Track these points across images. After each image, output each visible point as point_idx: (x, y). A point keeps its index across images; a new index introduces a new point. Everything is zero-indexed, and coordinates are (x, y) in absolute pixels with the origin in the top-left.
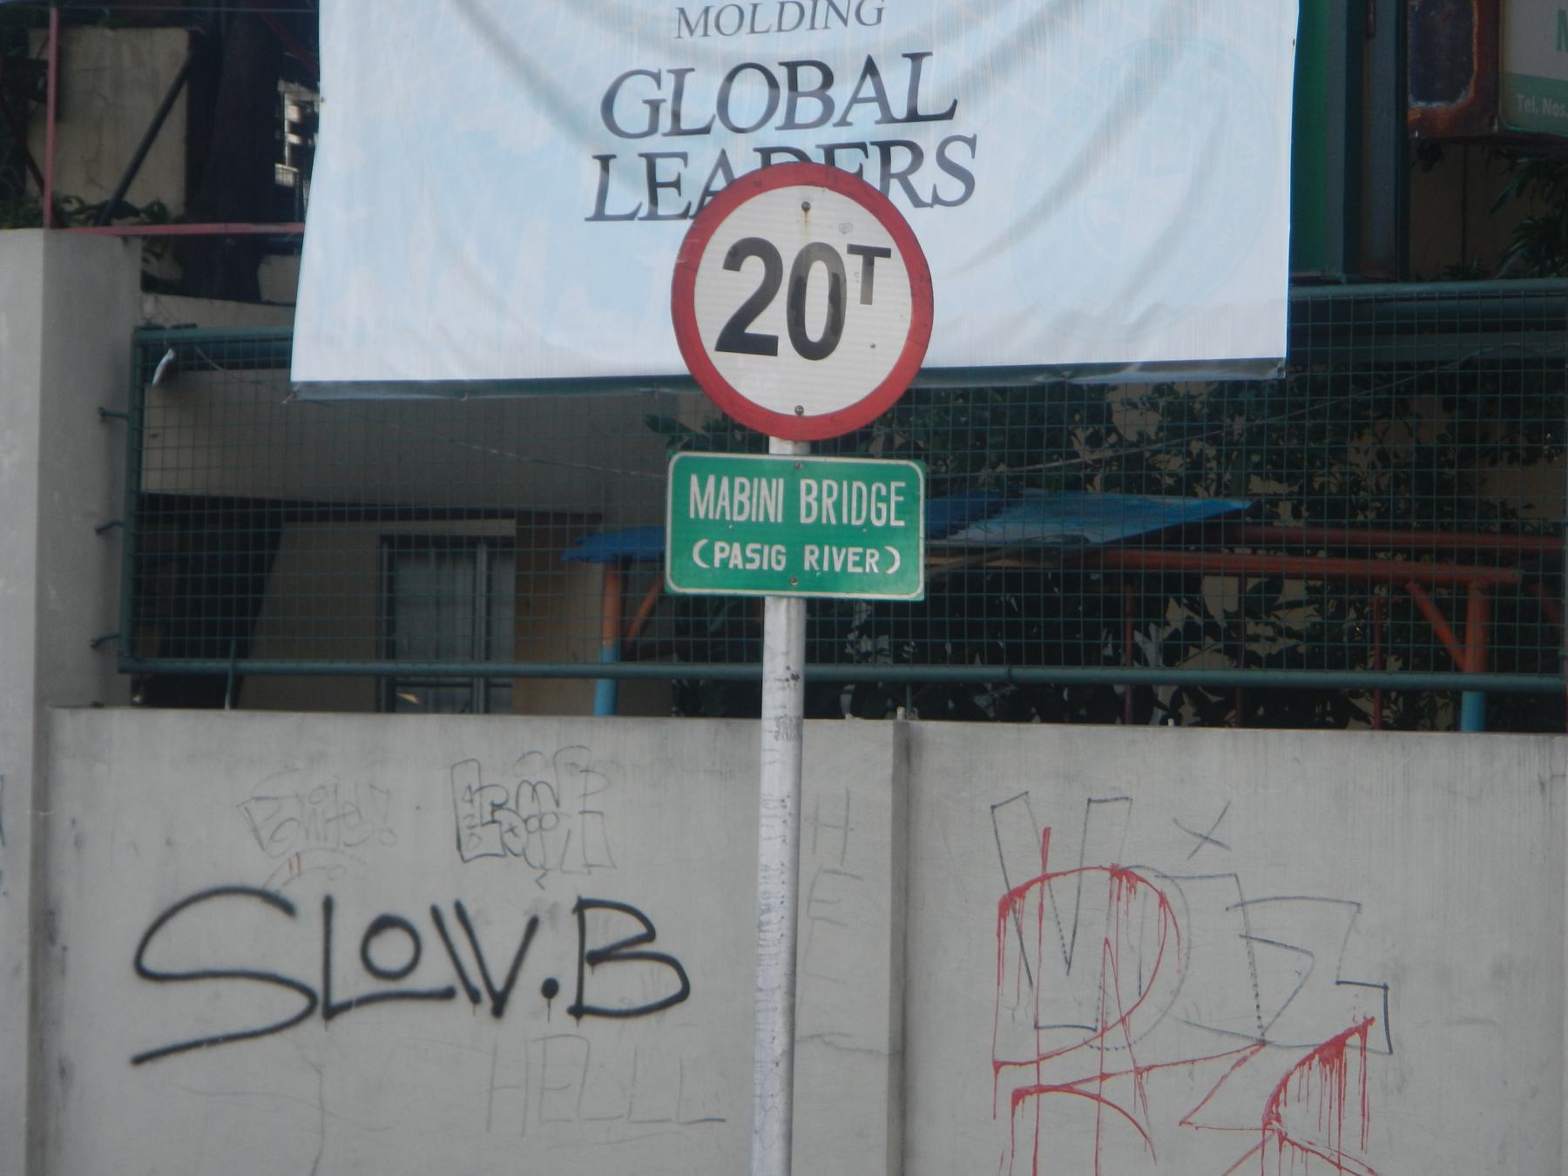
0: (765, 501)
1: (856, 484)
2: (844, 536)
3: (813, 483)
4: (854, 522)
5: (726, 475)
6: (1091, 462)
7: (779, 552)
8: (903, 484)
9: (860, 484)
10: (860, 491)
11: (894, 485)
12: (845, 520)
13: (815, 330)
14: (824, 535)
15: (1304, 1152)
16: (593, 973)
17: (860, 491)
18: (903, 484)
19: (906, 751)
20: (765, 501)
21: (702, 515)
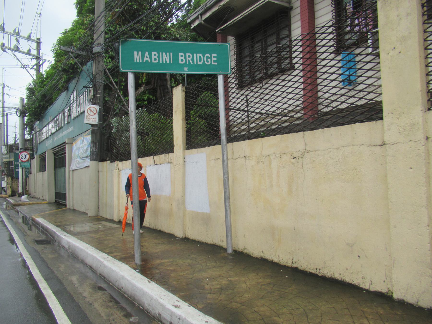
0: (165, 59)
1: (198, 55)
2: (26, 165)
3: (183, 54)
4: (199, 63)
5: (147, 51)
6: (10, 178)
7: (182, 60)
8: (216, 55)
9: (201, 55)
10: (200, 57)
11: (213, 55)
12: (195, 63)
13: (25, 156)
14: (25, 165)
15: (72, 208)
16: (430, 137)
17: (200, 57)
18: (216, 55)
19: (43, 173)
20: (165, 59)
21: (138, 61)
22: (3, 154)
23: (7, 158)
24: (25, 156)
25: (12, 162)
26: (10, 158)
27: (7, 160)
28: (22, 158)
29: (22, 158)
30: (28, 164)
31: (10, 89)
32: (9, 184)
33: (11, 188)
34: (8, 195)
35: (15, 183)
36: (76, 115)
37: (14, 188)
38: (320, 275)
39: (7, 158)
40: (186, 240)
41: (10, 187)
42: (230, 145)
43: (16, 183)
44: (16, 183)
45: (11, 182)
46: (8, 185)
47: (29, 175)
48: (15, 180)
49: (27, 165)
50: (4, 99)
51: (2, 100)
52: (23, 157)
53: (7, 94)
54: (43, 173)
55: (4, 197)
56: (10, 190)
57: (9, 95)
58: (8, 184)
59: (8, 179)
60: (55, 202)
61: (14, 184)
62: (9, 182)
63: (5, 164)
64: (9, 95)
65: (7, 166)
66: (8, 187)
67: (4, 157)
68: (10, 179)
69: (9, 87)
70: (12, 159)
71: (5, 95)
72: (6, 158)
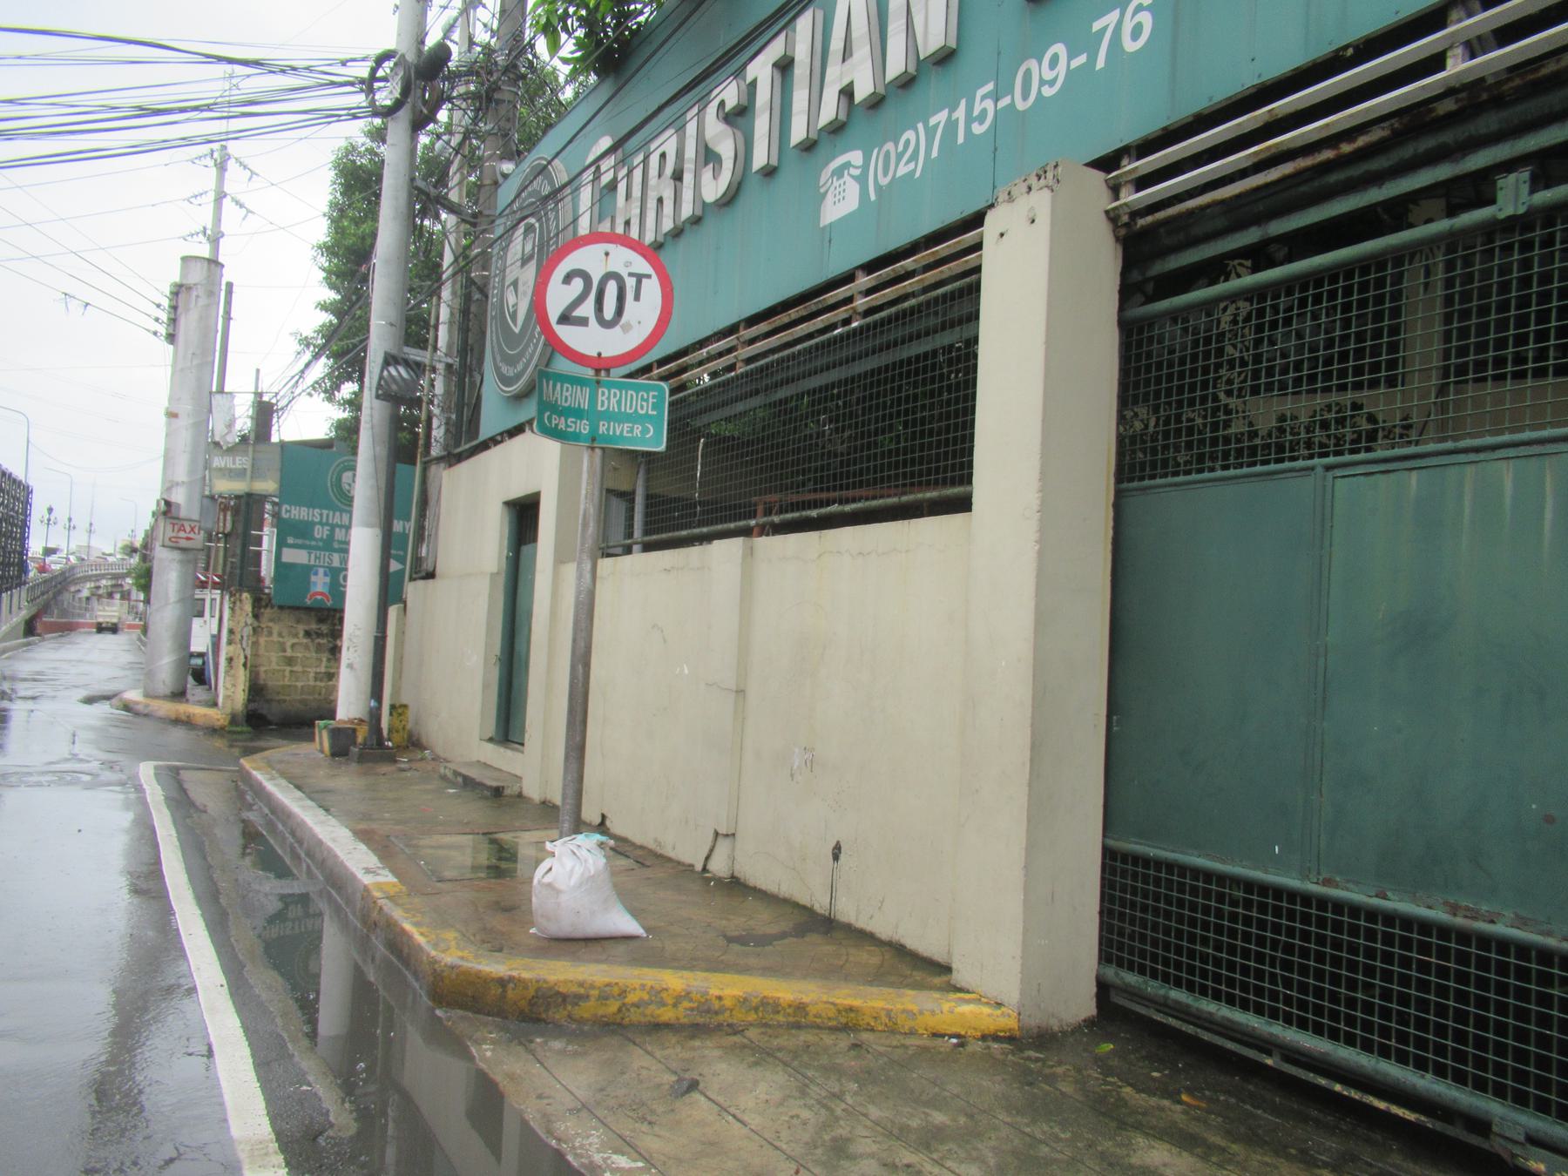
2: (620, 418)
13: (612, 289)
14: (609, 416)
19: (750, 553)
22: (217, 444)
23: (239, 474)
24: (612, 289)
25: (260, 499)
26: (256, 472)
27: (239, 487)
28: (565, 319)
29: (565, 319)
30: (646, 409)
31: (250, 179)
32: (238, 637)
33: (245, 665)
34: (229, 710)
35: (270, 634)
36: (668, 225)
37: (262, 669)
38: (1112, 1000)
39: (239, 474)
40: (485, 764)
41: (243, 660)
42: (412, 583)
43: (275, 638)
44: (275, 638)
45: (248, 631)
46: (231, 648)
47: (413, 590)
48: (271, 620)
49: (634, 418)
50: (220, 220)
51: (209, 226)
52: (587, 309)
53: (237, 203)
54: (750, 553)
55: (200, 721)
56: (242, 677)
57: (242, 206)
58: (230, 642)
59: (232, 609)
60: (1086, 1007)
61: (262, 640)
62: (238, 630)
63: (225, 509)
64: (242, 206)
65: (234, 522)
66: (230, 660)
67: (218, 462)
68: (248, 607)
69: (245, 167)
70: (268, 486)
71: (227, 202)
72: (231, 470)
